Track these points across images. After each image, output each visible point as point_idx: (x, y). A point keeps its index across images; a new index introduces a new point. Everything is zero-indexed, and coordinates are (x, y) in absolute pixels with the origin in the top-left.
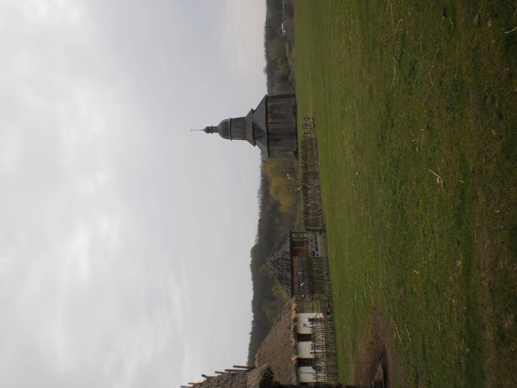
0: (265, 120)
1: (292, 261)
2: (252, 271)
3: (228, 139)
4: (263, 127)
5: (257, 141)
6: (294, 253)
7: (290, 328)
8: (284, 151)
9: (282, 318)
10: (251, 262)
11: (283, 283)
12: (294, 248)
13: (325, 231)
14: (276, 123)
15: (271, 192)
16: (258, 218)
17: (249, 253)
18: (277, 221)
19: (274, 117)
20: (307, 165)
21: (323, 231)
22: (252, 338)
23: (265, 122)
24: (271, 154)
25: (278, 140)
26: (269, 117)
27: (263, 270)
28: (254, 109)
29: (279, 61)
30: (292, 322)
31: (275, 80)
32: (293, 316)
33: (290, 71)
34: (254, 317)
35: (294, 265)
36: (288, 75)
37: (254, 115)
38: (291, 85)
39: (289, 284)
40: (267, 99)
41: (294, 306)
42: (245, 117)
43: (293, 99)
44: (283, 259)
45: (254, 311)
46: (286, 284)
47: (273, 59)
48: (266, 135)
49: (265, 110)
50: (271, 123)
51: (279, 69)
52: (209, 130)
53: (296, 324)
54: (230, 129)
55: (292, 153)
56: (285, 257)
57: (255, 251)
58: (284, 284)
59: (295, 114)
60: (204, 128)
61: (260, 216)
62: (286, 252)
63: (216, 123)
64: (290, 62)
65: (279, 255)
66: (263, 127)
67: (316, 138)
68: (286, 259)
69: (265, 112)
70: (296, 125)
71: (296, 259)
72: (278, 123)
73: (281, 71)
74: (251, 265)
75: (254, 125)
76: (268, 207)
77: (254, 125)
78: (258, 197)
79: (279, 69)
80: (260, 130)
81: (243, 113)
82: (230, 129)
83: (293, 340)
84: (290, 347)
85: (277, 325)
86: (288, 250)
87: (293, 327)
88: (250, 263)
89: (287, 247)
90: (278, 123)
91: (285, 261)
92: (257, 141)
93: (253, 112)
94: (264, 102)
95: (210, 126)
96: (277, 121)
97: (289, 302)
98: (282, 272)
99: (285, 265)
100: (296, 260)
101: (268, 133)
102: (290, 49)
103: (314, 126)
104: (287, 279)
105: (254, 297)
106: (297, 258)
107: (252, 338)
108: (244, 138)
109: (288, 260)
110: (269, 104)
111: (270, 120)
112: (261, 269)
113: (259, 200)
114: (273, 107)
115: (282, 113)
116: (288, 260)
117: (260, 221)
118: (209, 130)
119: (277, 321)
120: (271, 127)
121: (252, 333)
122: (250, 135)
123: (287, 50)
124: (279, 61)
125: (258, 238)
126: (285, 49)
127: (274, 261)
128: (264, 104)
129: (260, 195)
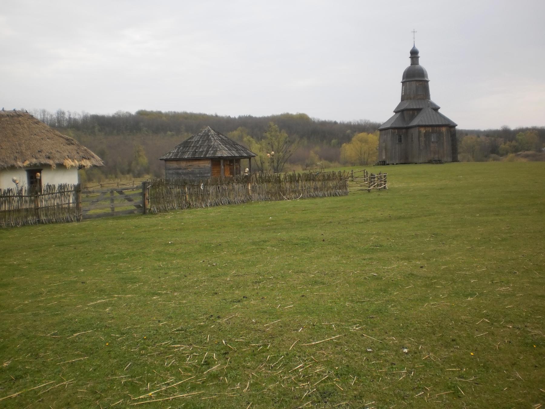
0: (424, 124)
1: (205, 159)
2: (282, 115)
3: (403, 79)
4: (415, 122)
5: (398, 114)
6: (216, 161)
7: (49, 158)
8: (386, 149)
9: (70, 147)
10: (291, 114)
11: (179, 148)
12: (222, 162)
13: (144, 213)
14: (419, 137)
15: (363, 135)
16: (338, 121)
17: (302, 112)
18: (334, 141)
19: (427, 135)
20: (298, 181)
21: (143, 211)
22: (212, 116)
23: (421, 123)
24: (383, 131)
25: (400, 140)
26: (428, 129)
27: (270, 126)
28: (439, 111)
29: (514, 143)
30: (57, 162)
31: (493, 139)
32: (69, 163)
33: (502, 155)
34: (235, 119)
35: (201, 162)
36: (498, 153)
37: (430, 110)
38: (486, 156)
39: (177, 155)
40: (451, 126)
41: (87, 163)
42: (429, 99)
43: (450, 159)
44: (209, 146)
45: (240, 118)
46: (178, 152)
47: (517, 137)
48: (405, 126)
49: (437, 123)
50: (420, 132)
51: (505, 143)
52: (414, 54)
53: (54, 166)
54: (415, 81)
55: (384, 157)
56: (210, 149)
57: (303, 119)
58: (178, 150)
59: (430, 162)
60: (418, 48)
61: (340, 123)
62: (217, 151)
63: (422, 63)
64: (511, 155)
65: (215, 142)
66: (415, 122)
67: (346, 194)
68: (207, 151)
69: (434, 123)
70: (416, 163)
71: (207, 165)
72: (419, 140)
73: (503, 146)
74: (288, 114)
75: (419, 110)
76: (349, 131)
77: (419, 110)
78: (361, 120)
79: (505, 143)
80: (412, 117)
81: (435, 97)
82: (415, 81)
83: (27, 163)
84: (16, 159)
85: (61, 140)
86: (219, 154)
87: (51, 162)
88: (290, 112)
89: (224, 152)
90: (419, 140)
91: (205, 149)
92: (398, 114)
93: (436, 109)
94: (447, 123)
95: (419, 55)
96: (422, 139)
97: (95, 156)
98: (194, 146)
99: (201, 150)
100: (207, 165)
101: (408, 128)
102: (526, 156)
103: (369, 191)
104: (184, 153)
105: (256, 118)
106: (210, 165)
107: (211, 117)
108: (403, 99)
109: (206, 155)
110: (444, 129)
111: (423, 130)
112: (272, 124)
113: (358, 122)
114: (440, 134)
115: (432, 145)
116: (206, 155)
117: (335, 123)
118: (414, 54)
119: (67, 140)
120: (412, 131)
121: (217, 116)
122: (407, 105)
123: (526, 152)
124: (514, 143)
125: (316, 121)
126: (527, 150)
127: (209, 136)
128: (444, 123)
129: (363, 123)
